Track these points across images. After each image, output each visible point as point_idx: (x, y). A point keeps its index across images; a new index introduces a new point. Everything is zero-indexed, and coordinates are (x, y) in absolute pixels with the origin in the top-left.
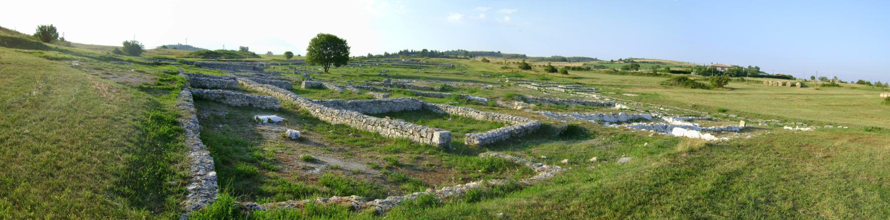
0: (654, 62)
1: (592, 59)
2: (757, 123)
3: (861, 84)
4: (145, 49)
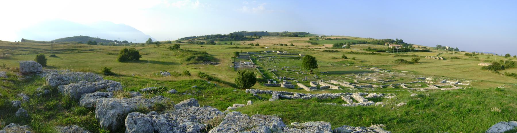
0: (342, 39)
1: (306, 33)
2: (292, 94)
3: (466, 55)
4: (153, 42)
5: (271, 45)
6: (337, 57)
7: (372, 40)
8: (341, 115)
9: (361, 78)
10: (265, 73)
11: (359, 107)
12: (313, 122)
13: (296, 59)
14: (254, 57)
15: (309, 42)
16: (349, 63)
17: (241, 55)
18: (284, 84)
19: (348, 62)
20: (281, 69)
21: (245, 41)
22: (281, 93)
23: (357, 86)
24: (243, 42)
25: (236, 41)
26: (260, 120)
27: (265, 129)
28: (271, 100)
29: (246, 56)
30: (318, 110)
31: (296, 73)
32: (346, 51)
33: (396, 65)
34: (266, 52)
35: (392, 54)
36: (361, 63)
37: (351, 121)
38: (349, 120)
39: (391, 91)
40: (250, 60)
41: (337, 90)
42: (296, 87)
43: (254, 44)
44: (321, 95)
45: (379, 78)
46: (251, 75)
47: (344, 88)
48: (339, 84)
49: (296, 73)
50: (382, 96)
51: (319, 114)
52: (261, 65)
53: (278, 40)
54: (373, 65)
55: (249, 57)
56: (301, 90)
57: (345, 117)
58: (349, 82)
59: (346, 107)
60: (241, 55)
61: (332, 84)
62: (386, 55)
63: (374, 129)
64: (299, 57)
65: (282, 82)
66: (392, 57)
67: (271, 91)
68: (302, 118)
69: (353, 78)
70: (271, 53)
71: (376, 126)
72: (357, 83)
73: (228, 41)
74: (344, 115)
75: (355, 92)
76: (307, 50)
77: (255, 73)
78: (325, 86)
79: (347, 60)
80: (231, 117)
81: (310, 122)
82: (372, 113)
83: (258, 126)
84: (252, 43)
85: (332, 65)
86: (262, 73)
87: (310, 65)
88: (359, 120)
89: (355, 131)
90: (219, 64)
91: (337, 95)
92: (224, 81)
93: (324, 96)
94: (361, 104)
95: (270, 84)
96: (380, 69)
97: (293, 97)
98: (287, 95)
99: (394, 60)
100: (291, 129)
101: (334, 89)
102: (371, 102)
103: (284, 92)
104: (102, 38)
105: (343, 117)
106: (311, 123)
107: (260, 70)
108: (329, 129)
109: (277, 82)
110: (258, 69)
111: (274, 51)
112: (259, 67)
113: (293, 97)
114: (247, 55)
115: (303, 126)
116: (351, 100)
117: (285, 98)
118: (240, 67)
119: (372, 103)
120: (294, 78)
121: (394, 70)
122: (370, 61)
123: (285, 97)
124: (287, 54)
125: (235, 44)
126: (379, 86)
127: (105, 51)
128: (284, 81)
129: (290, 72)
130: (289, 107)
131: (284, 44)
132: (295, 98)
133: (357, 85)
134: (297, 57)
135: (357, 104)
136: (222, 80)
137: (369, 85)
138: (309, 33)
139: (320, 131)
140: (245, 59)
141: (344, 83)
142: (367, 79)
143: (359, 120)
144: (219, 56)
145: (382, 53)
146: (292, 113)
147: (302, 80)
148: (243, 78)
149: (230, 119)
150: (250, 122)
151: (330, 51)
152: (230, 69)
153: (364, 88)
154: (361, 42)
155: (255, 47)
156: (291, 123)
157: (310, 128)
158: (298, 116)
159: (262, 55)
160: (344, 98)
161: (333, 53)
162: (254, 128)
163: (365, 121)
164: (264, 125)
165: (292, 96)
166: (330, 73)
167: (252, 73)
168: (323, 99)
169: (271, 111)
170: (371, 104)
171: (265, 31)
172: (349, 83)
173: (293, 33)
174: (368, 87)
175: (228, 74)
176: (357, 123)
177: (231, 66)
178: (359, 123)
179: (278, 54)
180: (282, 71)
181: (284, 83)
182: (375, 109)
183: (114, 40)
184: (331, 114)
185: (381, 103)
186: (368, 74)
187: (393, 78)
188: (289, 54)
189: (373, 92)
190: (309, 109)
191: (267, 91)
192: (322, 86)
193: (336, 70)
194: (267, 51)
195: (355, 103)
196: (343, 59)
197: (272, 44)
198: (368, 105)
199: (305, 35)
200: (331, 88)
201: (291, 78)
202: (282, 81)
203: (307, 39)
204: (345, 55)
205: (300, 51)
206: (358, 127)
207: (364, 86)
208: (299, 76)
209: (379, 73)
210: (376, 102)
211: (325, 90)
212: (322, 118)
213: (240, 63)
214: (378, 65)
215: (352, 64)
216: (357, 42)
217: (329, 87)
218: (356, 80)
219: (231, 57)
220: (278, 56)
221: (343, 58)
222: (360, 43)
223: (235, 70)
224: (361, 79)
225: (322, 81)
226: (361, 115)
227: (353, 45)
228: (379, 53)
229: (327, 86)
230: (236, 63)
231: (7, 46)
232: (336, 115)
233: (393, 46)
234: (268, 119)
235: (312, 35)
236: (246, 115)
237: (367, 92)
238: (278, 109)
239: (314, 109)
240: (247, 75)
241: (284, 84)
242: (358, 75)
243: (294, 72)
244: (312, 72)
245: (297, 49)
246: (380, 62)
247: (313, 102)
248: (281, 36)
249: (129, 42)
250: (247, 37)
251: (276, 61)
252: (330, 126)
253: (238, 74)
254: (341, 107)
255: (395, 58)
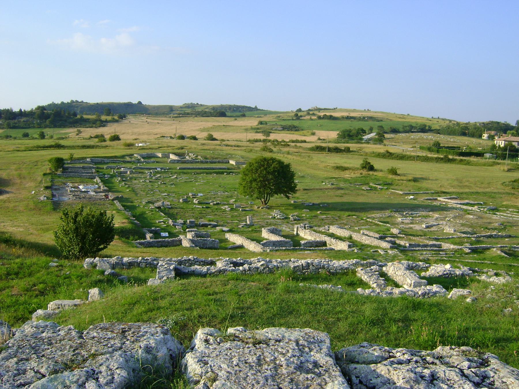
1: (250, 107)
2: (213, 263)
5: (152, 138)
6: (346, 165)
7: (444, 124)
8: (353, 317)
9: (412, 223)
10: (138, 214)
11: (403, 299)
12: (283, 329)
13: (222, 173)
14: (105, 171)
15: (256, 130)
16: (381, 182)
17: (71, 168)
18: (190, 239)
19: (377, 180)
20: (181, 200)
21: (82, 129)
22: (180, 263)
23: (399, 245)
24: (76, 129)
25: (56, 129)
26: (109, 339)
27: (121, 359)
28: (153, 282)
29: (83, 168)
30: (295, 301)
31: (223, 208)
32: (371, 151)
33: (514, 194)
34: (139, 157)
35: (504, 164)
36: (413, 183)
37: (380, 335)
38: (375, 331)
39: (495, 264)
40: (95, 178)
41: (344, 251)
42: (223, 245)
43: (106, 137)
44: (303, 262)
45: (463, 225)
46: (98, 219)
47: (363, 247)
48: (351, 238)
49: (223, 208)
50: (468, 275)
51: (298, 311)
52: (127, 193)
53: (171, 125)
54: (447, 191)
55: (94, 171)
56: (237, 251)
57: (364, 323)
58: (377, 232)
59: (368, 297)
60: (70, 165)
61: (332, 236)
62: (484, 165)
63: (445, 357)
64: (228, 169)
65: (185, 233)
66: (504, 170)
67: (155, 260)
68: (252, 319)
69: (388, 223)
70: (152, 160)
71: (451, 349)
72: (401, 237)
73: (34, 127)
74: (362, 318)
75: (393, 259)
76: (251, 151)
77: (109, 213)
78: (313, 239)
79: (375, 173)
80: (28, 338)
81: (278, 328)
82: (437, 318)
83: (102, 354)
84: (99, 134)
85: (333, 186)
86: (127, 213)
87: (260, 188)
88: (401, 332)
89: (392, 359)
90: (7, 192)
91: (346, 266)
92: (24, 241)
93: (311, 266)
94: (408, 291)
95: (151, 240)
96: (466, 201)
97: (214, 271)
98: (197, 267)
99: (507, 180)
100: (229, 344)
101: (336, 249)
102: (435, 288)
103: (190, 260)
105: (360, 322)
106: (280, 331)
107: (124, 206)
108: (325, 350)
109: (171, 235)
110: (117, 204)
111: (160, 155)
112: (122, 197)
113: (213, 269)
114: (86, 165)
115: (257, 337)
116: (381, 281)
117: (194, 274)
118: (68, 198)
119: (437, 290)
120: (217, 222)
121: (507, 207)
122: (436, 180)
123: (194, 271)
124: (198, 162)
125: (52, 137)
126: (461, 247)
128: (189, 231)
129: (207, 208)
130: (200, 296)
131: (188, 134)
132: (221, 272)
133: (398, 242)
134: (225, 169)
135: (397, 292)
136: (18, 237)
137: (431, 243)
138: (256, 109)
139: (303, 352)
140: (81, 177)
141: (363, 234)
142: (427, 227)
143: (401, 332)
144: (8, 171)
145: (473, 159)
146: (211, 311)
147: (240, 226)
148: (77, 228)
149: (25, 343)
150: (81, 346)
151: (330, 150)
152: (40, 205)
153: (419, 250)
154: (415, 128)
155: (108, 143)
156: (227, 327)
157: (277, 343)
158: (241, 313)
159: (128, 165)
160: (362, 274)
161: (339, 155)
162: (93, 360)
163: (418, 337)
164: (121, 348)
165: (213, 267)
166: (327, 207)
167: (101, 214)
168: (307, 272)
169: (151, 310)
170: (435, 293)
171: (135, 101)
172: (377, 236)
173: (214, 108)
174: (429, 248)
175: (34, 220)
176: (396, 339)
177: (42, 198)
178: (402, 340)
179: (173, 162)
180: (185, 206)
181: (189, 236)
182: (446, 308)
184: (329, 312)
185: (465, 292)
186: (431, 213)
187: (505, 228)
188: (202, 162)
189: (444, 262)
190: (271, 297)
191: (143, 259)
192: (306, 239)
193: (346, 199)
194: (141, 155)
195: (392, 289)
196: (365, 172)
197: (156, 136)
198: (426, 296)
199: (247, 113)
200: (328, 247)
201: (210, 221)
202: (185, 230)
203: (253, 122)
204: (369, 161)
205: (233, 152)
206: (400, 349)
207: (419, 246)
208: (232, 216)
209: (461, 213)
210: (452, 288)
211: (312, 250)
212: (305, 322)
213: (69, 189)
214: (461, 191)
215: (389, 184)
216: (404, 127)
217: (324, 244)
218: (397, 228)
219: (42, 173)
220: (172, 166)
221: (364, 168)
222: (410, 129)
223: (55, 209)
224: (411, 226)
225: (305, 227)
226: (407, 321)
227: (392, 136)
228: (464, 158)
229: (318, 239)
230: (56, 189)
232: (340, 316)
233: (505, 141)
234: (130, 332)
235: (266, 113)
236: (70, 329)
237: (427, 261)
238: (171, 305)
239: (285, 297)
240: (87, 222)
241: (191, 238)
242: (403, 215)
243: (216, 207)
244: (266, 204)
245: (224, 148)
246: (467, 184)
247: (283, 278)
248: (180, 114)
250: (85, 117)
251: (167, 181)
252: (328, 341)
253: (61, 218)
254: (354, 297)
255: (510, 174)
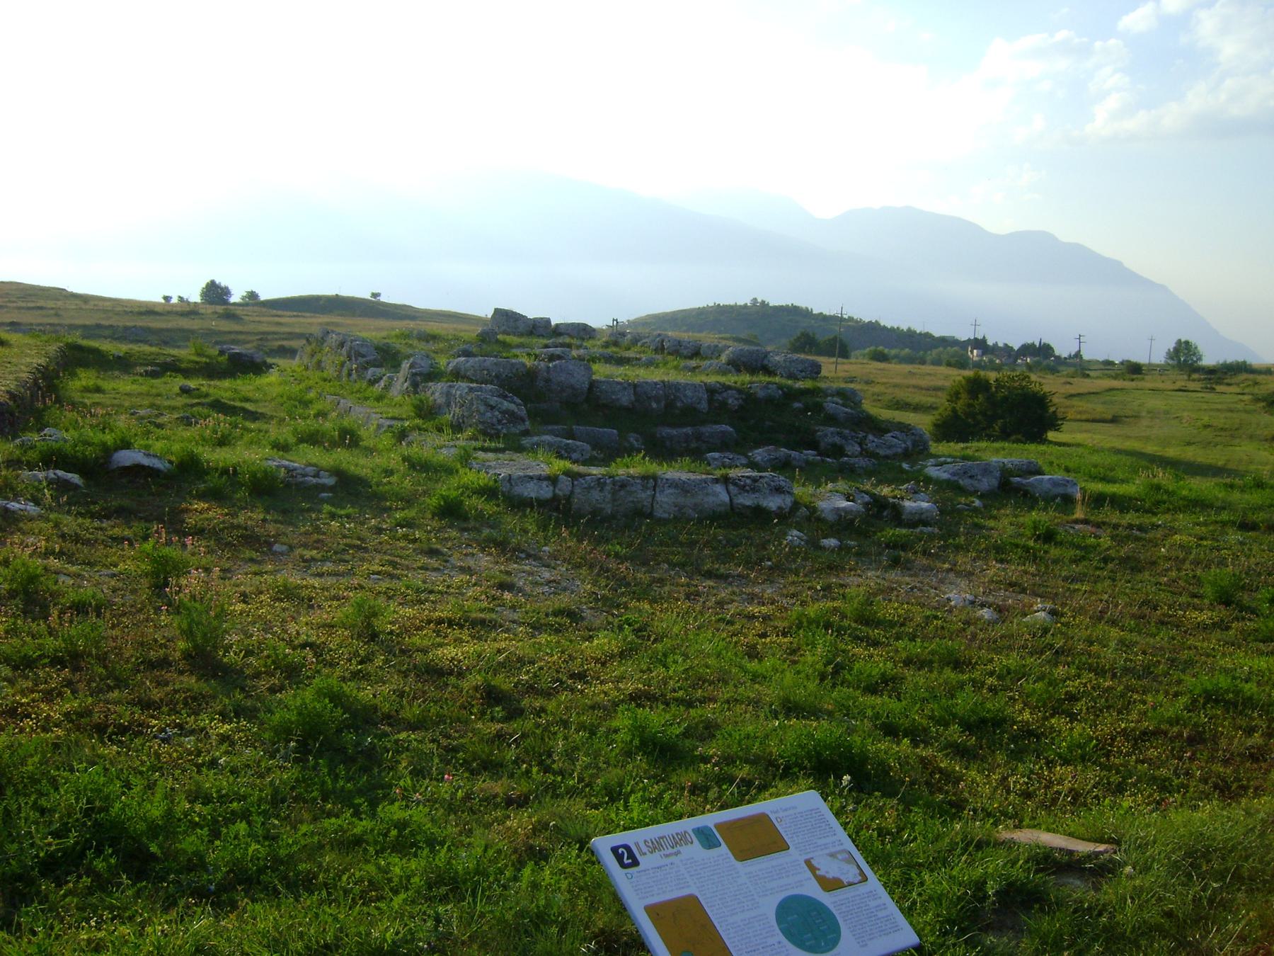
104: (888, 322)
127: (877, 389)
183: (964, 338)
231: (128, 324)
249: (1065, 355)
